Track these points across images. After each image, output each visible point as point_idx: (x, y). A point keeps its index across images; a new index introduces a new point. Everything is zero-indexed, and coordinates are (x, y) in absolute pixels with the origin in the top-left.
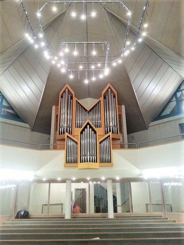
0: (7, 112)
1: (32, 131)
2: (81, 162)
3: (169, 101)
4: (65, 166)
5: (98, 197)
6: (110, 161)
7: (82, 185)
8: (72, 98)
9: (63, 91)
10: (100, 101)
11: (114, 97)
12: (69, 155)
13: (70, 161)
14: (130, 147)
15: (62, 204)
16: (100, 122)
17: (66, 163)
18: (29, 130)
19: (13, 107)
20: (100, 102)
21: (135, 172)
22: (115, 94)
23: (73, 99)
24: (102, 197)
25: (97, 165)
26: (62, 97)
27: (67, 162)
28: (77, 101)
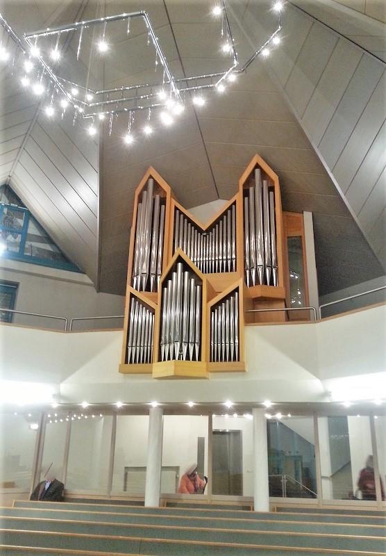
0: (39, 249)
1: (98, 292)
2: (160, 360)
5: (290, 452)
6: (236, 357)
8: (163, 202)
9: (144, 184)
10: (235, 203)
11: (271, 189)
12: (142, 342)
13: (135, 359)
16: (234, 256)
17: (126, 362)
18: (92, 291)
19: (52, 237)
20: (233, 206)
21: (311, 386)
22: (273, 181)
23: (165, 205)
24: (299, 454)
25: (200, 367)
26: (140, 200)
28: (176, 208)
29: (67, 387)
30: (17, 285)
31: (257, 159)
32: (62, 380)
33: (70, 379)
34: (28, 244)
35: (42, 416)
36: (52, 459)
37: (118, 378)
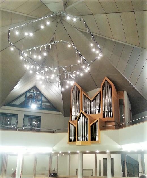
0: (46, 105)
1: (65, 117)
2: (78, 141)
3: (21, 96)
4: (68, 144)
6: (97, 140)
7: (105, 156)
8: (79, 92)
14: (117, 128)
15: (93, 169)
17: (69, 141)
19: (49, 101)
26: (73, 92)
27: (70, 141)
28: (83, 94)
29: (55, 148)
30: (41, 117)
31: (106, 78)
32: (54, 146)
33: (56, 146)
34: (43, 104)
35: (51, 156)
36: (54, 167)
37: (68, 146)
